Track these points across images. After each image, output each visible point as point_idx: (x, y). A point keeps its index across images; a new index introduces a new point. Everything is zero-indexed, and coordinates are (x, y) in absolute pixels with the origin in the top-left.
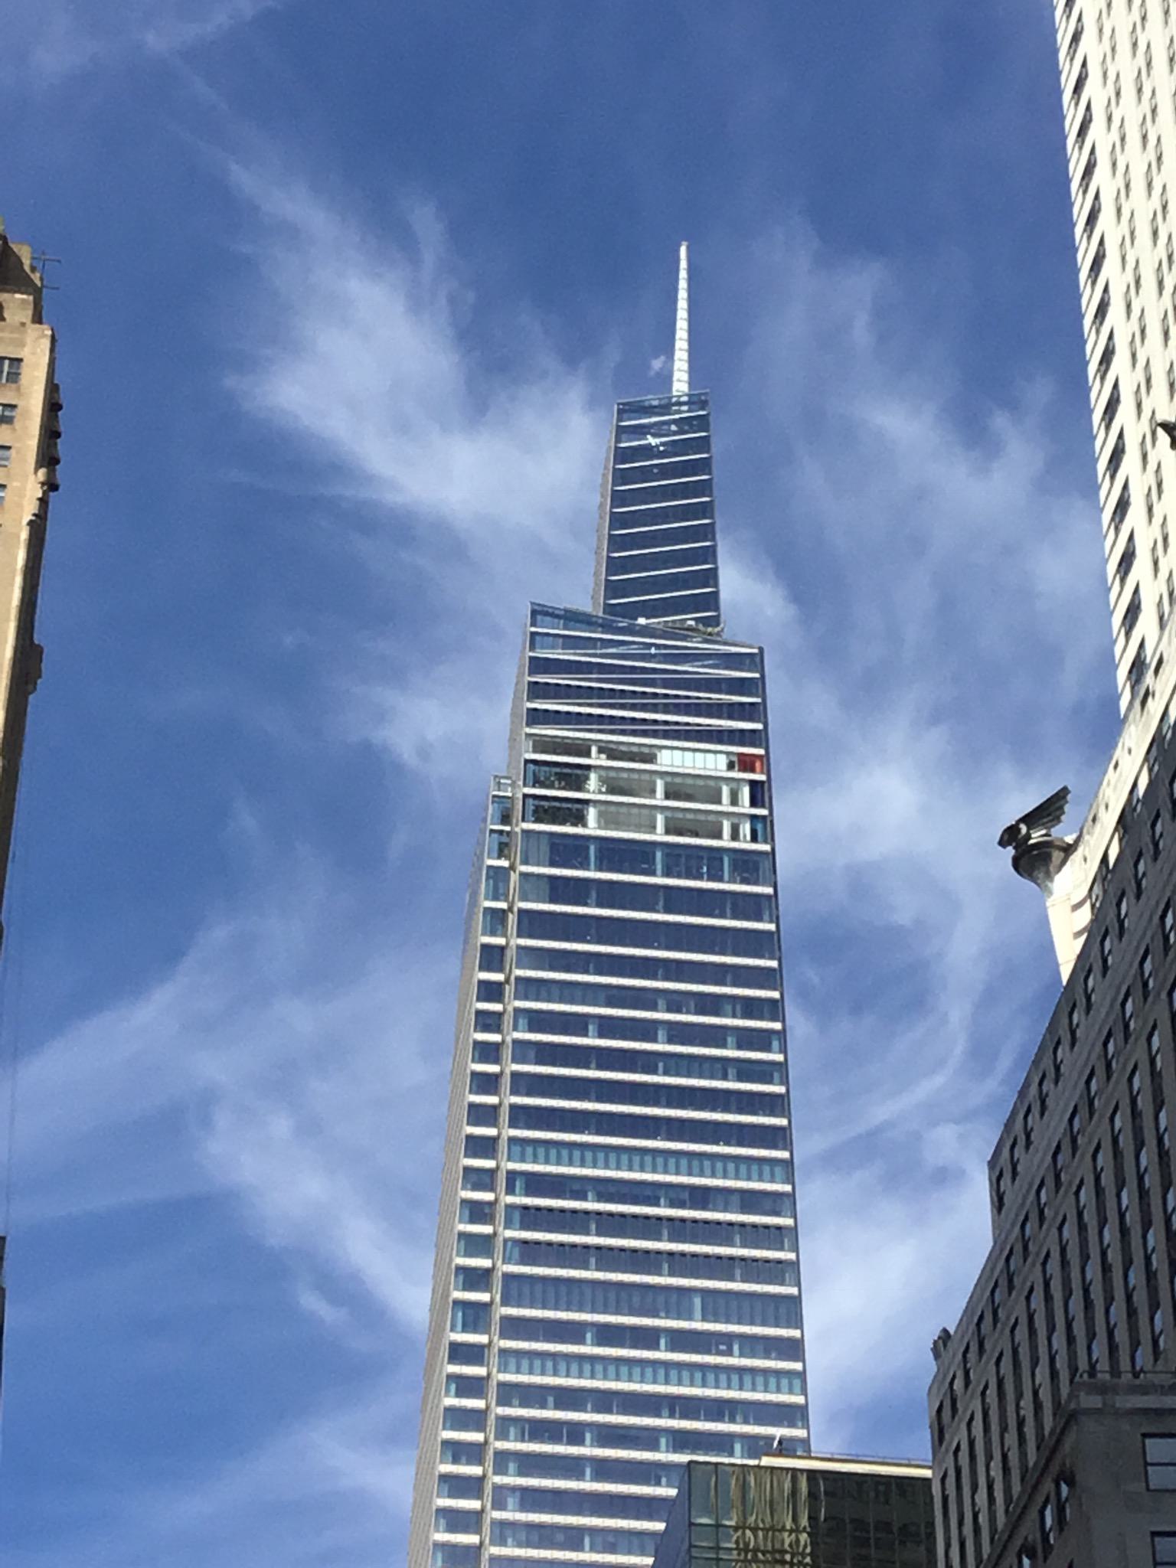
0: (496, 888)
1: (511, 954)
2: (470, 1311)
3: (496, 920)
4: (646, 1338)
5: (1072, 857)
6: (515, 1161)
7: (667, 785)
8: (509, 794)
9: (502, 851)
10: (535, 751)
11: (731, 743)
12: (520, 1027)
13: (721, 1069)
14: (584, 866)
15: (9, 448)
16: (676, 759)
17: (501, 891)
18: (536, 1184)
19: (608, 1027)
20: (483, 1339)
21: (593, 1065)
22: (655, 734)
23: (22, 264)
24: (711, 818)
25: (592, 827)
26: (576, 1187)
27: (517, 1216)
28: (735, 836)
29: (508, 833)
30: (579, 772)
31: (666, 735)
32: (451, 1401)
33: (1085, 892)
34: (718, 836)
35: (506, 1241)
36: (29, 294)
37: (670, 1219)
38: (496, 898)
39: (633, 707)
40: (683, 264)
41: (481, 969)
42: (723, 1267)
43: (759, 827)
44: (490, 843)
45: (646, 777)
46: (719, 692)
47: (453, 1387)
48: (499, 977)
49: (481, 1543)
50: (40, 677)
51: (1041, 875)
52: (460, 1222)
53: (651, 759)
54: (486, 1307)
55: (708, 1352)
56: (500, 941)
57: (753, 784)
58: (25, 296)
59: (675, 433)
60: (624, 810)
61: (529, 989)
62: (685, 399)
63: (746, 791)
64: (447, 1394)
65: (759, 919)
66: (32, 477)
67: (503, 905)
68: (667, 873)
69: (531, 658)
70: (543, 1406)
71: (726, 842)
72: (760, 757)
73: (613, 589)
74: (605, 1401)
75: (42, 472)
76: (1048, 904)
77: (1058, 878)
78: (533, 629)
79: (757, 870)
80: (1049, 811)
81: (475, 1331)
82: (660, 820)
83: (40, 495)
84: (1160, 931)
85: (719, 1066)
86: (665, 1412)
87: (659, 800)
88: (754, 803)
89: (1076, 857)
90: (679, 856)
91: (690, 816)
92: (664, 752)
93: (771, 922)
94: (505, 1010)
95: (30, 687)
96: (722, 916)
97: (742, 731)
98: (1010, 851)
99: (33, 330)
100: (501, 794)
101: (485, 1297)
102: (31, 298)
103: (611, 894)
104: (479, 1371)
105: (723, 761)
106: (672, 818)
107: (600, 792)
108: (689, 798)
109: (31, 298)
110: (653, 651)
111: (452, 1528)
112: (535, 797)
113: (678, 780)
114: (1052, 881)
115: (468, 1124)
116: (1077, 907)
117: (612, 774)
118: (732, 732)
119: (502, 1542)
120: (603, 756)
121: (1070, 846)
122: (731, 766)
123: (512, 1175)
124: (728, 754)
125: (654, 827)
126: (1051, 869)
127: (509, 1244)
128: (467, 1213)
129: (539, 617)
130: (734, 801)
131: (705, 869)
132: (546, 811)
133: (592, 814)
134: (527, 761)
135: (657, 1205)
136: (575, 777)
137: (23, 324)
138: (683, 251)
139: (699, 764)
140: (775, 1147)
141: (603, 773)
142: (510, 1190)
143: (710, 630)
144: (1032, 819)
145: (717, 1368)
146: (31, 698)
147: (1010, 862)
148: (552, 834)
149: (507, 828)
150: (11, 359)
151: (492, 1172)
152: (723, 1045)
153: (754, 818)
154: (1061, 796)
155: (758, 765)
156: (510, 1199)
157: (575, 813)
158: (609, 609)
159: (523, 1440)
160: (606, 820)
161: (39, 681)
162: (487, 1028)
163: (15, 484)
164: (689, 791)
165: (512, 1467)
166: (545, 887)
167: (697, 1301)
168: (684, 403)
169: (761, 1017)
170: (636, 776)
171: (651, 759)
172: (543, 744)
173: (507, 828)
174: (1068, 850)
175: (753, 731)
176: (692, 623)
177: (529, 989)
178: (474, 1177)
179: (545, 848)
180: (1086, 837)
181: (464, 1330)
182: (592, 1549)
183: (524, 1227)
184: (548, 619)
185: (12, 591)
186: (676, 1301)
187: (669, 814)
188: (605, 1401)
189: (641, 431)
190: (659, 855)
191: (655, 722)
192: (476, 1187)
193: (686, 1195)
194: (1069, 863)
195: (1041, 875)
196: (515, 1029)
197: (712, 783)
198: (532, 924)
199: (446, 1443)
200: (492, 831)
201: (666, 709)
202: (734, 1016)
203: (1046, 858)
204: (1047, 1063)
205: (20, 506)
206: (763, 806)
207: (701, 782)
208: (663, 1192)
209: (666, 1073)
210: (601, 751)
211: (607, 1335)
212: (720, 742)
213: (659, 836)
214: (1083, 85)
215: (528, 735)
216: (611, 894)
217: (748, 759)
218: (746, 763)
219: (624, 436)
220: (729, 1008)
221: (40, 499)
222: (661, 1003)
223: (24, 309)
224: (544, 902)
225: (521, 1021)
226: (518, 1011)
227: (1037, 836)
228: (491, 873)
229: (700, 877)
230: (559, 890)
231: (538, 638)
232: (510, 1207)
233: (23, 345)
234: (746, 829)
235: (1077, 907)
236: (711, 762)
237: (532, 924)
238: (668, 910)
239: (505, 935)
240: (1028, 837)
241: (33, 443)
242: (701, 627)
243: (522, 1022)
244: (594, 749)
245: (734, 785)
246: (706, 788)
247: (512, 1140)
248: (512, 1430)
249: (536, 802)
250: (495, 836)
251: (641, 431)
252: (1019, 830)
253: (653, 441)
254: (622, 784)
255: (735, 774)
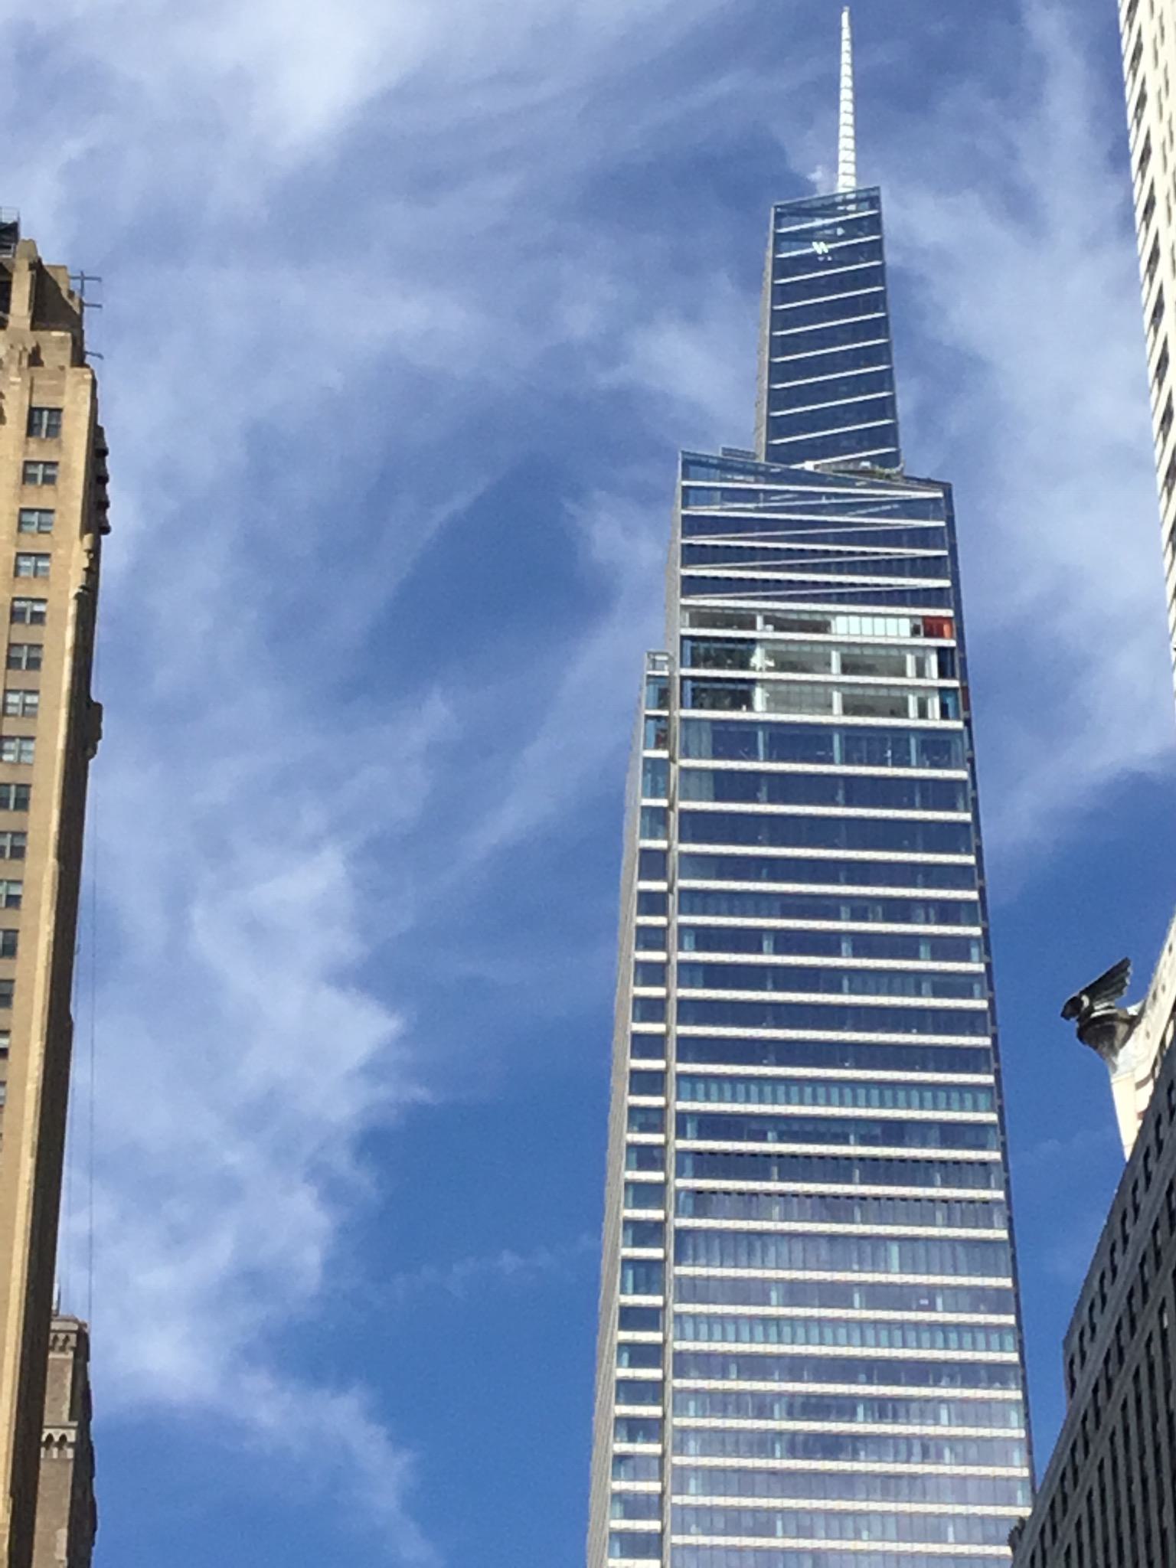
0: (654, 781)
1: (673, 861)
2: (642, 1270)
3: (656, 820)
4: (838, 1294)
5: (1136, 1030)
6: (686, 1100)
7: (843, 657)
8: (666, 673)
9: (661, 741)
10: (692, 626)
11: (915, 604)
12: (686, 946)
13: (913, 982)
14: (752, 756)
15: (51, 512)
16: (853, 626)
17: (661, 785)
18: (712, 1125)
19: (786, 942)
20: (657, 1300)
21: (770, 986)
22: (827, 599)
23: (58, 289)
24: (896, 693)
25: (760, 710)
26: (754, 1126)
27: (689, 1162)
28: (923, 713)
29: (666, 718)
30: (741, 647)
31: (841, 599)
32: (625, 1372)
33: (1147, 1071)
34: (903, 713)
35: (678, 1191)
36: (66, 330)
37: (862, 1159)
38: (655, 795)
39: (803, 568)
40: (846, 34)
41: (641, 877)
42: (923, 1211)
43: (949, 701)
44: (643, 730)
45: (820, 649)
46: (899, 545)
47: (626, 1356)
48: (661, 886)
49: (663, 1530)
50: (99, 737)
51: (1105, 1050)
52: (628, 1168)
53: (822, 627)
54: (659, 1264)
55: (909, 1309)
56: (661, 844)
57: (941, 651)
58: (61, 334)
59: (842, 238)
60: (796, 688)
61: (694, 901)
62: (852, 196)
63: (933, 660)
64: (619, 1365)
65: (953, 808)
66: (78, 542)
67: (663, 803)
68: (847, 760)
69: (684, 517)
70: (725, 1376)
71: (912, 721)
72: (948, 619)
73: (776, 427)
74: (795, 1368)
75: (88, 537)
76: (1113, 1080)
77: (1122, 1052)
78: (686, 483)
79: (948, 751)
80: (1109, 983)
81: (648, 1292)
82: (837, 698)
83: (86, 564)
84: (1166, 1210)
85: (911, 980)
86: (862, 1377)
87: (835, 675)
88: (942, 674)
89: (1140, 1030)
90: (859, 739)
91: (871, 692)
92: (840, 619)
93: (966, 810)
94: (669, 924)
95: (90, 751)
96: (911, 806)
97: (927, 590)
98: (1074, 1024)
99: (73, 375)
100: (657, 673)
101: (657, 1253)
102: (69, 335)
103: (784, 788)
104: (655, 1337)
105: (905, 626)
106: (852, 696)
107: (769, 669)
108: (870, 670)
109: (69, 335)
110: (824, 501)
111: (629, 1515)
112: (694, 679)
113: (857, 651)
114: (1116, 1053)
115: (632, 1057)
116: (1140, 1085)
117: (781, 647)
118: (916, 592)
119: (684, 1531)
120: (770, 627)
121: (1133, 1017)
122: (915, 632)
123: (682, 1117)
124: (911, 617)
125: (830, 706)
126: (1117, 1043)
127: (682, 1195)
128: (634, 1156)
129: (692, 468)
130: (921, 673)
131: (889, 753)
132: (703, 693)
133: (759, 695)
134: (683, 638)
135: (846, 1142)
136: (738, 654)
137: (62, 368)
138: (845, 17)
139: (880, 631)
140: (976, 1071)
141: (770, 647)
142: (681, 1133)
143: (887, 471)
144: (1094, 991)
145: (917, 1325)
146: (91, 762)
147: (1075, 1034)
148: (715, 722)
149: (665, 713)
150: (51, 410)
151: (661, 1111)
152: (915, 956)
153: (942, 691)
154: (1121, 969)
155: (946, 628)
156: (681, 1144)
157: (741, 696)
158: (773, 453)
159: (704, 1417)
160: (776, 701)
161: (100, 743)
162: (648, 946)
163: (60, 552)
164: (869, 662)
165: (692, 1445)
166: (708, 784)
167: (894, 1249)
168: (851, 202)
169: (957, 922)
170: (807, 649)
171: (822, 627)
172: (702, 617)
173: (665, 713)
174: (1133, 1022)
175: (940, 589)
176: (866, 464)
177: (694, 901)
178: (640, 1118)
179: (707, 739)
180: (1148, 1012)
181: (636, 1291)
182: (786, 1535)
183: (698, 1175)
184: (704, 470)
185: (62, 673)
186: (871, 1249)
187: (847, 691)
188: (795, 1368)
189: (808, 236)
190: (836, 739)
191: (828, 584)
192: (644, 1129)
193: (878, 1131)
194: (1133, 1037)
195: (1105, 1050)
196: (681, 948)
197: (894, 652)
198: (696, 826)
199: (619, 1420)
200: (648, 717)
201: (840, 569)
202: (927, 921)
203: (1111, 1032)
204: (1106, 1262)
205: (68, 578)
206: (953, 677)
207: (882, 652)
208: (853, 1128)
209: (853, 991)
210: (767, 621)
211: (795, 1293)
212: (902, 603)
213: (837, 717)
214: (1148, 157)
215: (684, 607)
216: (784, 788)
217: (934, 623)
218: (932, 628)
219: (785, 244)
220: (921, 912)
221: (86, 569)
222: (844, 911)
223: (60, 349)
224: (708, 800)
225: (686, 940)
226: (682, 928)
227: (1100, 1010)
228: (649, 766)
229: (883, 763)
230: (726, 785)
231: (691, 492)
232: (681, 1154)
233: (61, 393)
234: (934, 704)
235: (1140, 1085)
236: (892, 628)
237: (696, 826)
238: (849, 803)
239: (667, 837)
240: (1091, 1010)
241: (77, 504)
242: (877, 468)
243: (688, 941)
244: (759, 620)
245: (920, 654)
246: (887, 659)
247: (681, 1076)
248: (692, 1405)
249: (695, 685)
250: (651, 722)
251: (808, 236)
252: (1082, 1003)
253: (820, 248)
254: (793, 658)
255: (921, 641)
